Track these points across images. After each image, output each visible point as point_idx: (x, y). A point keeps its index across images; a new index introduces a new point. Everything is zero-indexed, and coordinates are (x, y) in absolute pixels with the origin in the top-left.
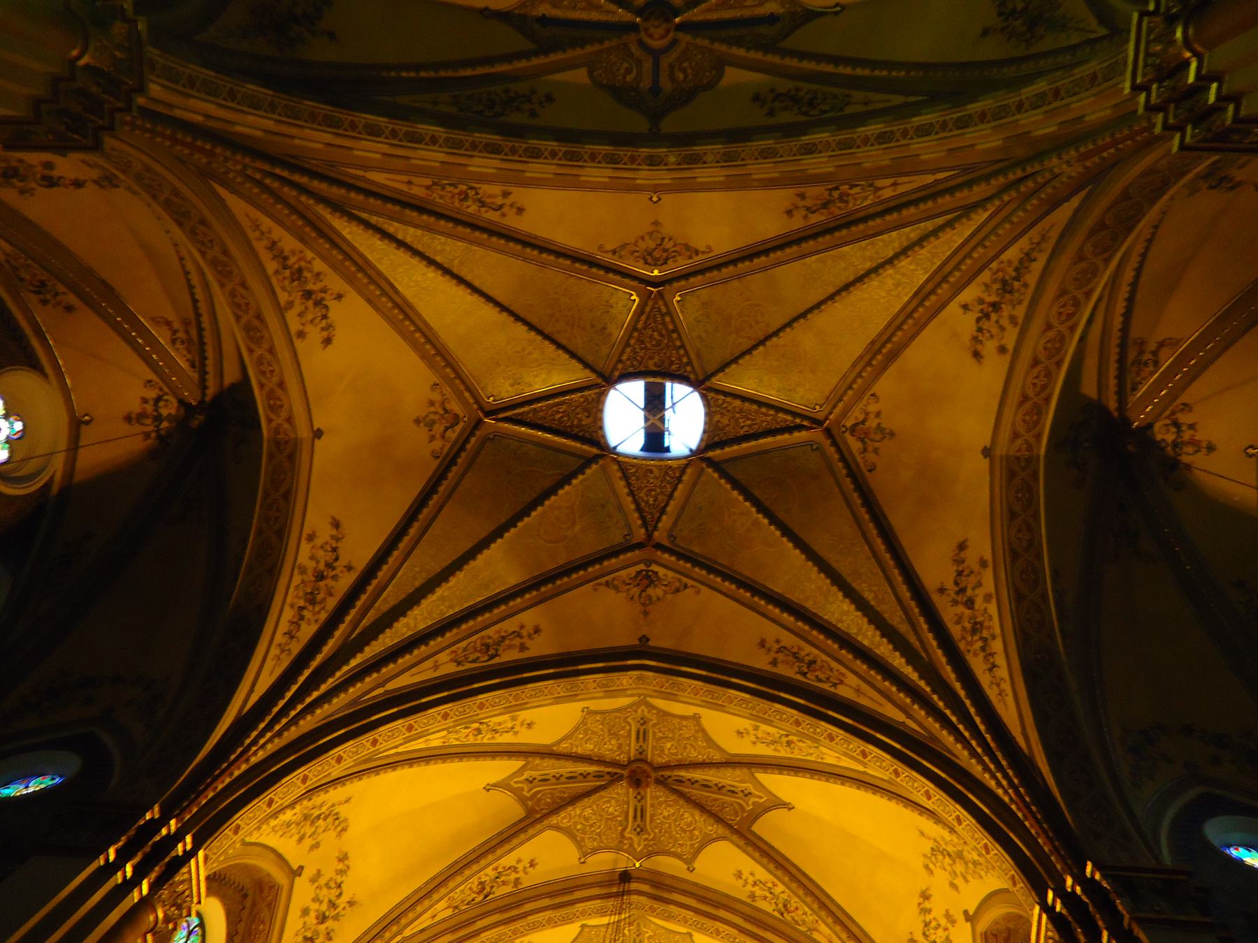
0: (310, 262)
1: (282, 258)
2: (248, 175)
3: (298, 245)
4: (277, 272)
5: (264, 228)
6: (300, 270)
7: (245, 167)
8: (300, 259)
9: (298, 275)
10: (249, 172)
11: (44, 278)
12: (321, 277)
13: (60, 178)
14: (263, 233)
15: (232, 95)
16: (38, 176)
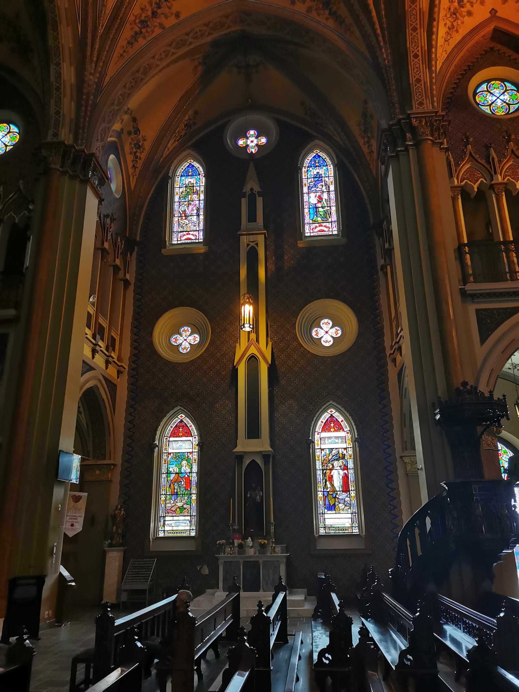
0: (136, 16)
1: (136, 35)
2: (95, 70)
3: (128, 26)
4: (144, 38)
5: (121, 51)
6: (141, 22)
7: (90, 74)
8: (135, 24)
9: (144, 23)
10: (93, 71)
11: (183, 125)
12: (143, 7)
13: (134, 128)
14: (124, 51)
15: (58, 89)
16: (135, 136)
